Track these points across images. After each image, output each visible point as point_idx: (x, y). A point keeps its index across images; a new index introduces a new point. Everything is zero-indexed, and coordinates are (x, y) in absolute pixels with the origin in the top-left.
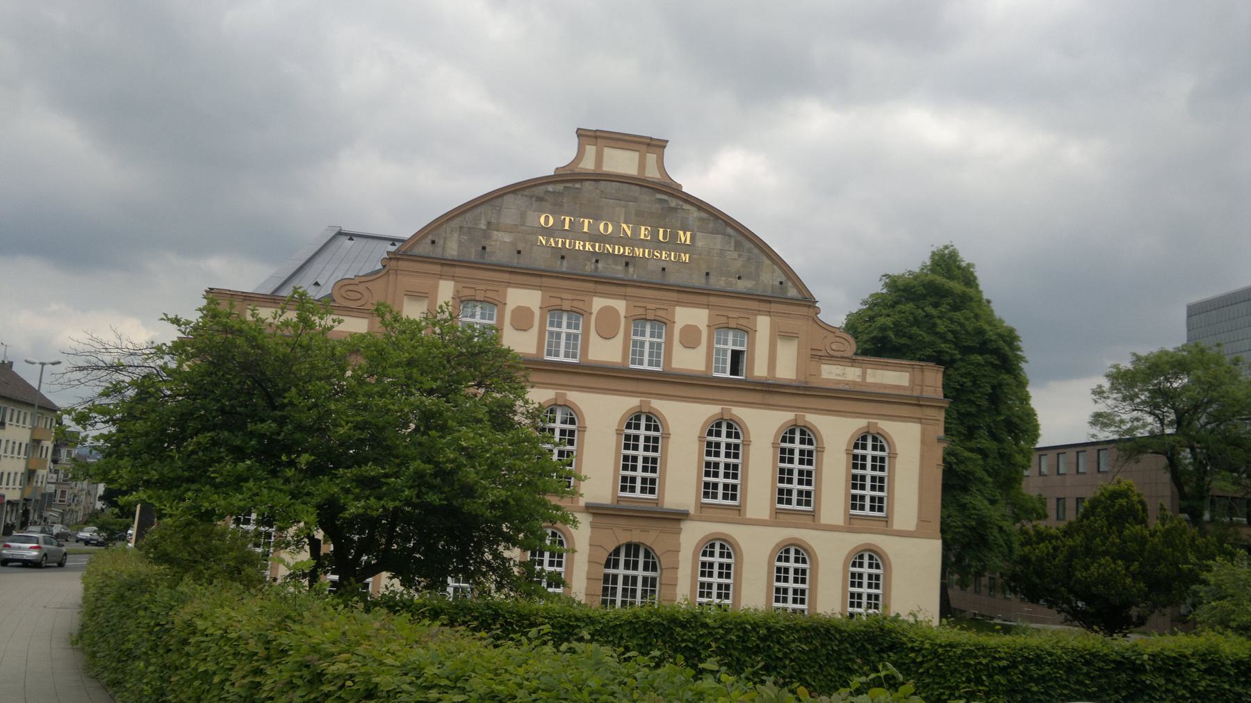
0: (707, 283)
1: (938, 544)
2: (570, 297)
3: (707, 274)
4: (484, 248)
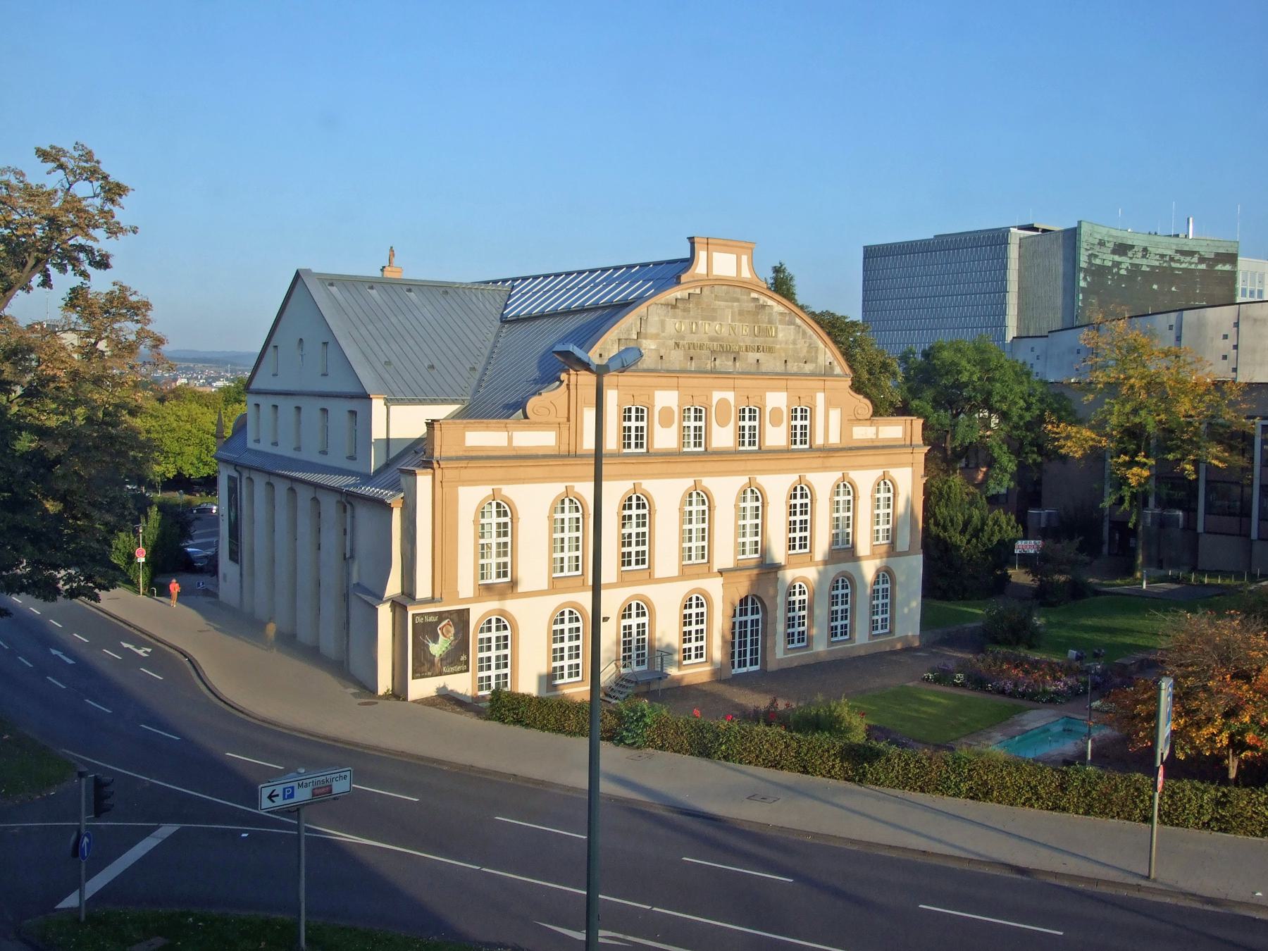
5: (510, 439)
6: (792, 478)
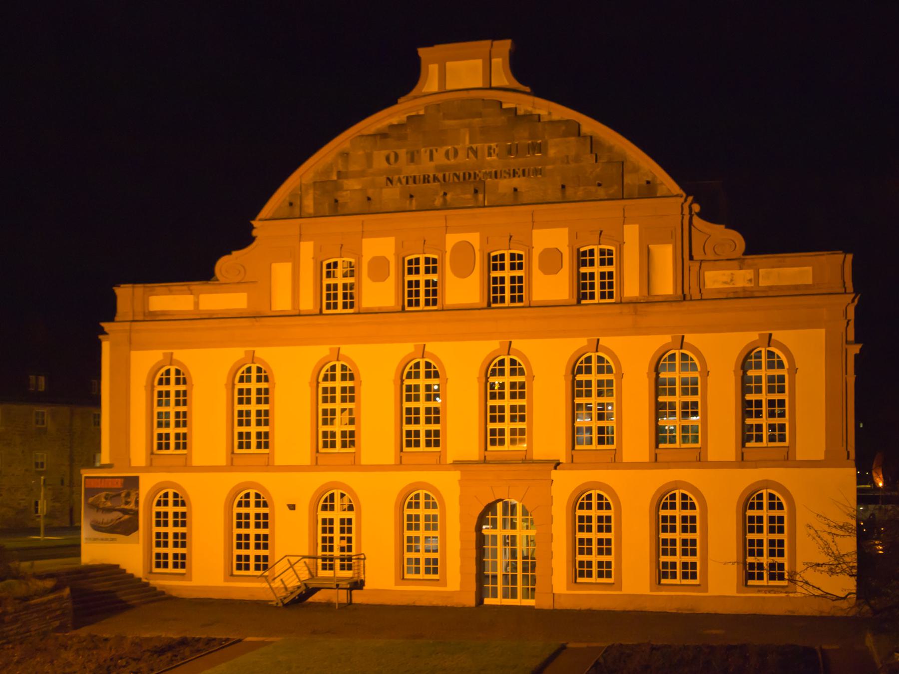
3: (563, 187)
5: (197, 304)
6: (404, 350)
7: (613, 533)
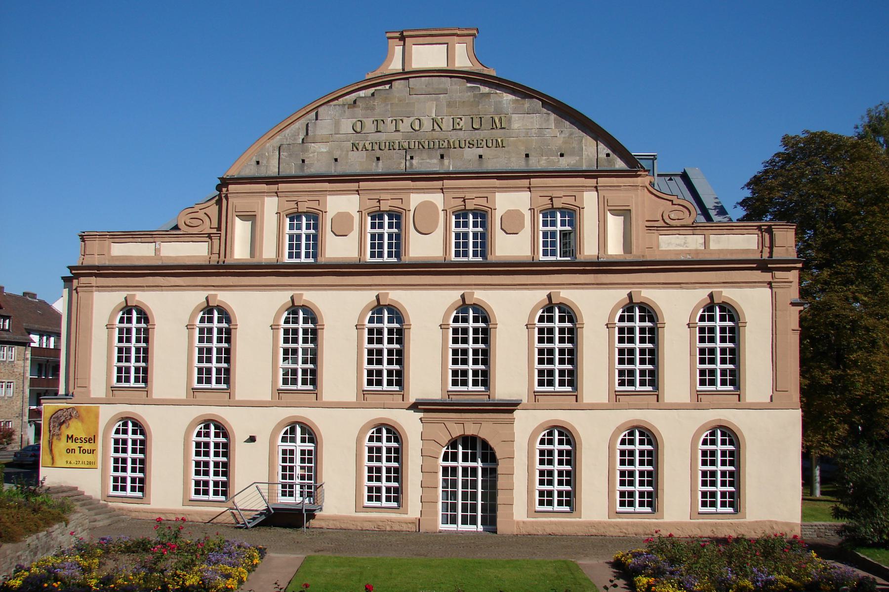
0: (527, 165)
1: (798, 413)
2: (389, 197)
3: (527, 156)
4: (303, 161)
7: (280, 449)
